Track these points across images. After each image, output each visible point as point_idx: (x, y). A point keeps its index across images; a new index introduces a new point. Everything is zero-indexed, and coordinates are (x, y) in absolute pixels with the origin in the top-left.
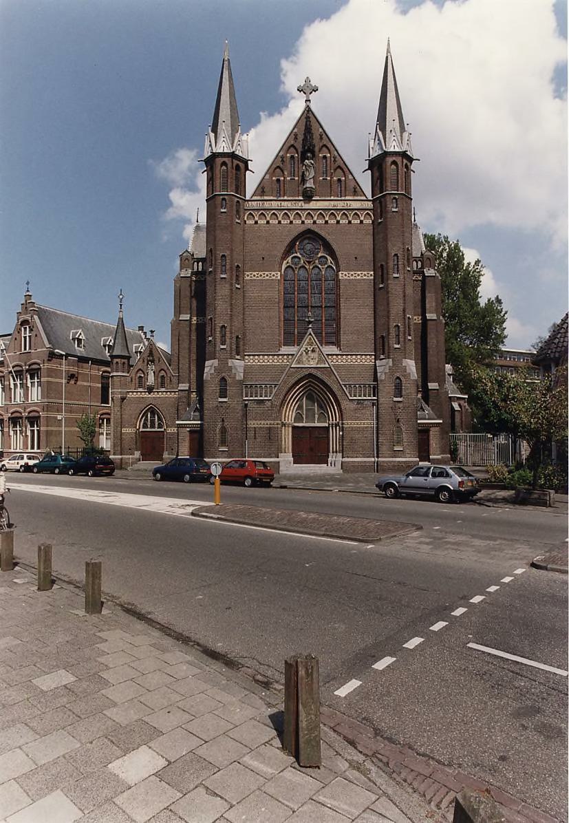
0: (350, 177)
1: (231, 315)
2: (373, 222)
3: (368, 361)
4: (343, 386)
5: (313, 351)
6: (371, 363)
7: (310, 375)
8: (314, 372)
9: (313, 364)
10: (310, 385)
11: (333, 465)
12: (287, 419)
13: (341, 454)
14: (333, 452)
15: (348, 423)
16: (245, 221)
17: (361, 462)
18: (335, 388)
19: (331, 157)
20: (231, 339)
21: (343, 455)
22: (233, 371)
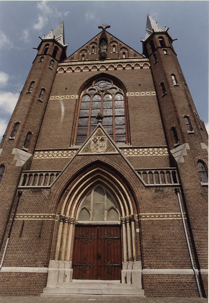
0: (131, 50)
1: (28, 115)
2: (150, 67)
3: (163, 153)
4: (136, 172)
5: (102, 140)
6: (164, 155)
7: (98, 163)
8: (103, 159)
9: (101, 151)
10: (99, 182)
11: (129, 282)
12: (68, 213)
13: (139, 263)
14: (128, 260)
15: (147, 216)
16: (57, 71)
17: (173, 275)
18: (127, 175)
19: (118, 45)
20: (22, 131)
21: (143, 264)
22: (15, 158)
